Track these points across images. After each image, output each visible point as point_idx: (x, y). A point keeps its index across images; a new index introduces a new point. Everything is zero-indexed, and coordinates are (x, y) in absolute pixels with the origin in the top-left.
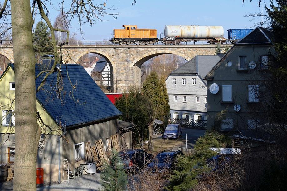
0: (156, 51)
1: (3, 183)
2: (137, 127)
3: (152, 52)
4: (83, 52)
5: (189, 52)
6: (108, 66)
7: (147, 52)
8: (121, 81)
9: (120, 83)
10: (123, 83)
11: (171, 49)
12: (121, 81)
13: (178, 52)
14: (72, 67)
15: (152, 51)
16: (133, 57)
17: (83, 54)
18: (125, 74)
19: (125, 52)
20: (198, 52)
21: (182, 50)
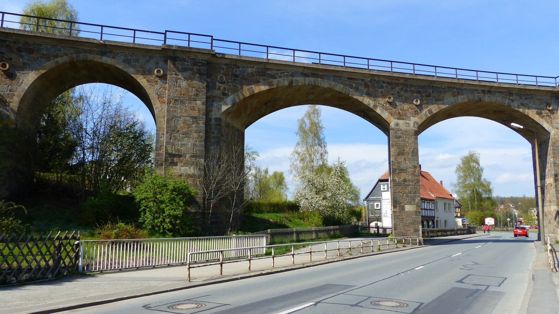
0: (290, 78)
1: (31, 241)
2: (212, 213)
3: (281, 79)
4: (57, 56)
5: (380, 90)
6: (215, 114)
7: (264, 80)
8: (180, 156)
9: (176, 164)
10: (185, 165)
11: (361, 69)
12: (180, 156)
13: (351, 87)
14: (371, 122)
15: (280, 77)
16: (222, 88)
17: (57, 62)
18: (195, 135)
19: (198, 70)
20: (402, 93)
21: (361, 85)
